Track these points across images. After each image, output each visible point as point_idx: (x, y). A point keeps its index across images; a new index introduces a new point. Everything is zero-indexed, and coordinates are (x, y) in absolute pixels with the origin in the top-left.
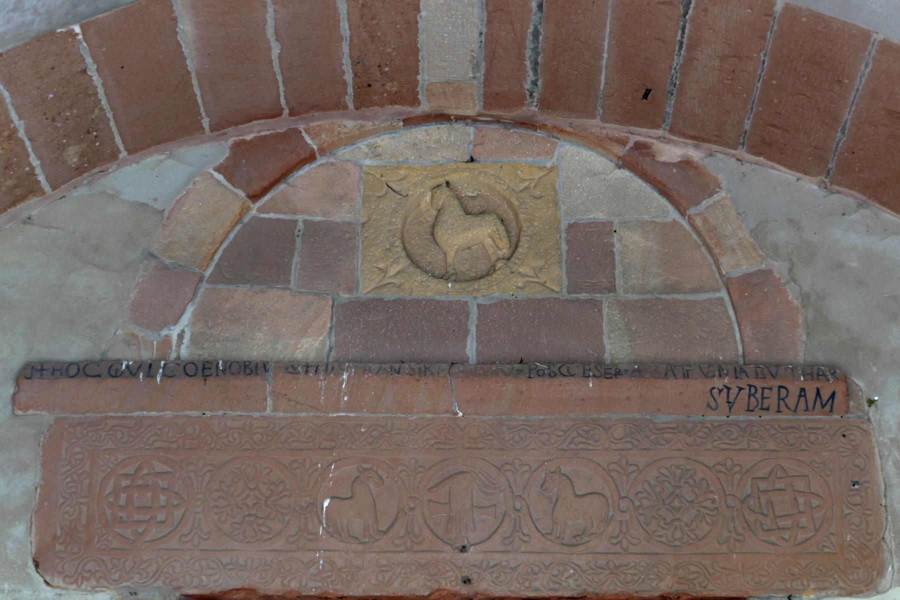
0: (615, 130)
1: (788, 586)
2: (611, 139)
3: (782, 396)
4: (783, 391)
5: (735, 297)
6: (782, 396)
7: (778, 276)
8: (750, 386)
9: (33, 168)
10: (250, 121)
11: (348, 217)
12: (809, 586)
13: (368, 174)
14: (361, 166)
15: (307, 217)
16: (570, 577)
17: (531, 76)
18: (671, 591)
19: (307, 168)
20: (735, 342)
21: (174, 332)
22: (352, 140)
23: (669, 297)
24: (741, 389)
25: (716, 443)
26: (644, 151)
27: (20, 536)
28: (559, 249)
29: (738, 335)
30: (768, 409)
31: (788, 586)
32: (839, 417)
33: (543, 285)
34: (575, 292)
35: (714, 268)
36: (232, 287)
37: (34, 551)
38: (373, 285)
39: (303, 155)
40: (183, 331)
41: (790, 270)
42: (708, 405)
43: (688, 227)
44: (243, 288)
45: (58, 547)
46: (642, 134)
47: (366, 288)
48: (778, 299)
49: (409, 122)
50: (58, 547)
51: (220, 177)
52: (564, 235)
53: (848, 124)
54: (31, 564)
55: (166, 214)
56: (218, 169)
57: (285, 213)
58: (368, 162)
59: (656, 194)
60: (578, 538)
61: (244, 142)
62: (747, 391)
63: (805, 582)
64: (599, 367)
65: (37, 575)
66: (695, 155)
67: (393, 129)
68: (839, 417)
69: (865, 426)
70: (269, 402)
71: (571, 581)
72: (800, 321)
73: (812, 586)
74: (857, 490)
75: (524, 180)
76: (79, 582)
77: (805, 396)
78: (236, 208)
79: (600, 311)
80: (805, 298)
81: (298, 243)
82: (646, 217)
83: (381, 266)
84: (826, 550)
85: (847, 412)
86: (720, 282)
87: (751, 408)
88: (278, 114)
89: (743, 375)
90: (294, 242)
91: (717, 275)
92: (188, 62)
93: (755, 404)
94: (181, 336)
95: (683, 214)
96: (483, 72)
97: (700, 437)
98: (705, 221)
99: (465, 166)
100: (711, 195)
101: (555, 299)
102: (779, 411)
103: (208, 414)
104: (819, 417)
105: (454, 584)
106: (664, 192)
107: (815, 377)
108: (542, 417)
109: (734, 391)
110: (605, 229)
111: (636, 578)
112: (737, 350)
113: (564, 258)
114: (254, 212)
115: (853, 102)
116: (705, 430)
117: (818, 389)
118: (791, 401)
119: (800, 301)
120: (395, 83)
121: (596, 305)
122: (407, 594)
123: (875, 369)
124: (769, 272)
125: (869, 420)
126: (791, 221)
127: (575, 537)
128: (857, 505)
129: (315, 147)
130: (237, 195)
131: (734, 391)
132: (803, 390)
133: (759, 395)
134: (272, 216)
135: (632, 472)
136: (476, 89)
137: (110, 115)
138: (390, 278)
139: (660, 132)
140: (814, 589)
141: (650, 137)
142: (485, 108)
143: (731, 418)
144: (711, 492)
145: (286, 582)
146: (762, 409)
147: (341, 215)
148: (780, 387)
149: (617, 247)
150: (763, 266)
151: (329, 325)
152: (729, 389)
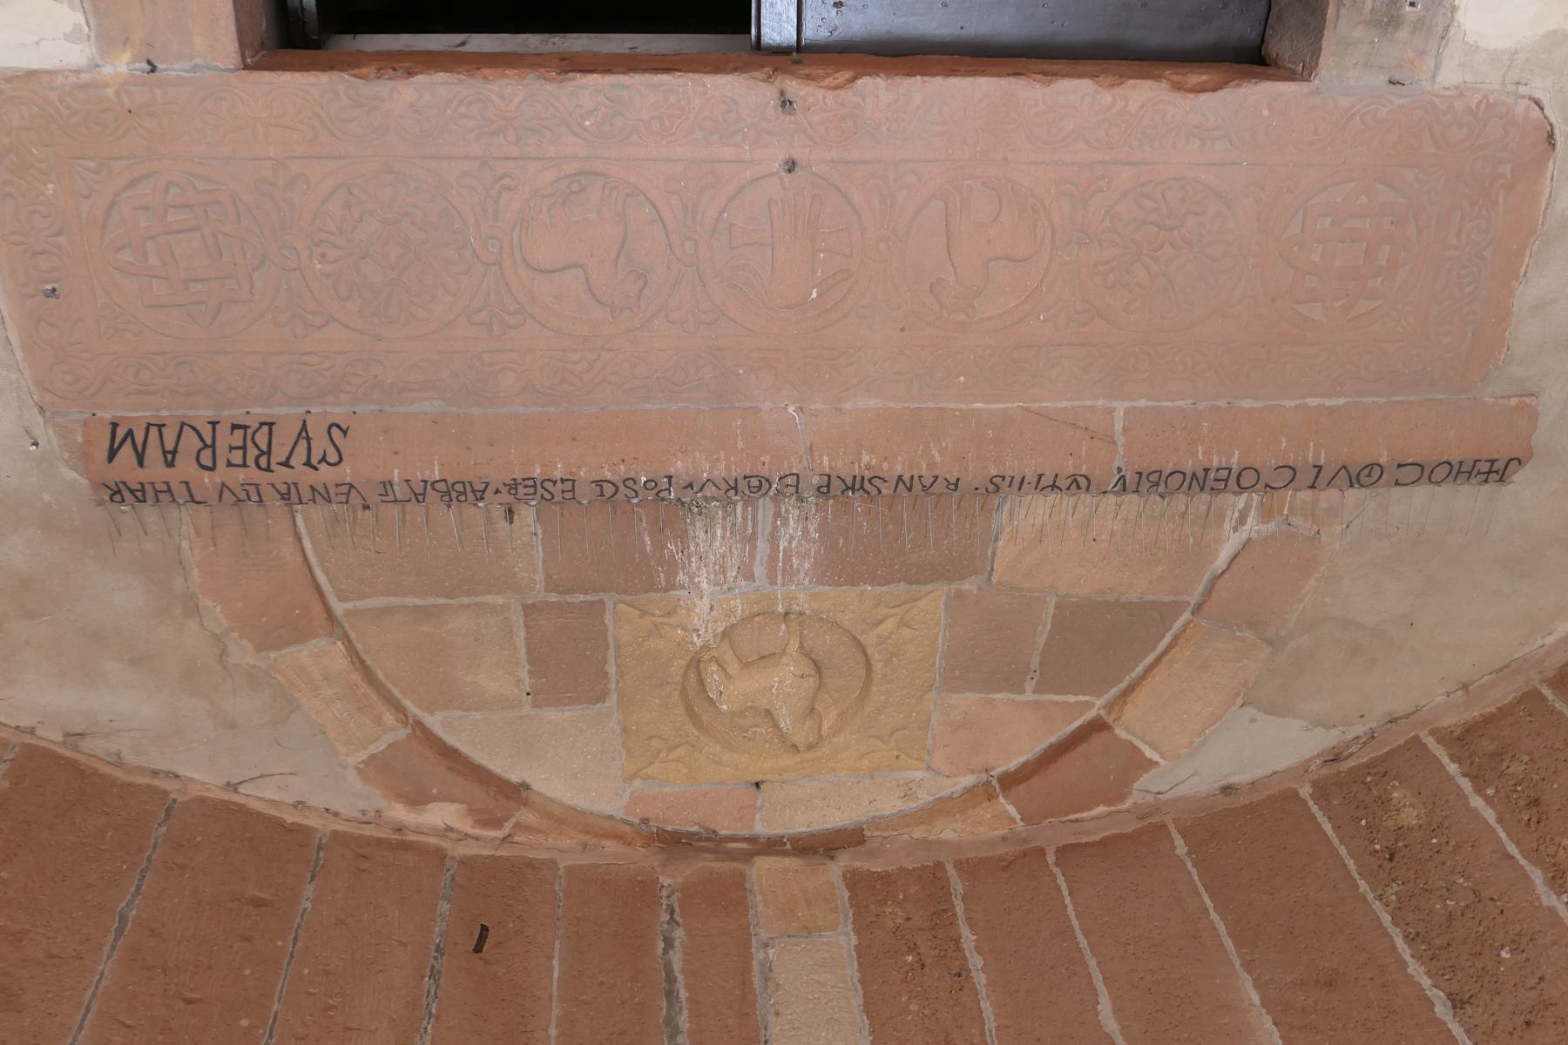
0: (537, 847)
1: (159, 93)
2: (539, 832)
3: (208, 452)
4: (206, 459)
5: (317, 608)
6: (208, 452)
7: (245, 642)
8: (268, 469)
9: (1479, 791)
10: (1104, 842)
11: (954, 699)
12: (117, 93)
13: (919, 759)
14: (929, 768)
15: (1018, 698)
16: (591, 112)
17: (677, 958)
18: (391, 84)
19: (1012, 765)
20: (310, 533)
21: (1252, 526)
22: (941, 808)
23: (431, 601)
24: (286, 464)
25: (326, 365)
26: (485, 816)
27: (1567, 193)
28: (618, 666)
29: (307, 544)
30: (234, 427)
31: (159, 93)
32: (100, 414)
33: (644, 613)
34: (594, 602)
35: (359, 647)
36: (1150, 597)
37: (1551, 164)
38: (921, 604)
39: (1021, 790)
40: (1235, 529)
41: (223, 653)
42: (345, 433)
43: (409, 704)
44: (1133, 597)
45: (1507, 170)
46: (484, 843)
47: (934, 600)
48: (240, 605)
49: (852, 838)
50: (1507, 170)
51: (1149, 754)
52: (613, 686)
53: (107, 949)
54: (1559, 139)
55: (1240, 701)
56: (1152, 764)
57: (1052, 702)
58: (918, 775)
59: (465, 749)
60: (575, 187)
61: (1108, 803)
62: (274, 460)
63: (126, 100)
64: (547, 496)
65: (1553, 120)
66: (400, 812)
67: (875, 823)
68: (100, 414)
69: (48, 398)
70: (1118, 426)
71: (589, 104)
72: (196, 573)
73: (110, 92)
74: (47, 282)
75: (678, 760)
76: (1483, 105)
77: (165, 453)
78: (1131, 712)
79: (548, 577)
80: (193, 609)
81: (1035, 662)
82: (478, 716)
83: (906, 632)
84: (92, 164)
85: (85, 423)
86: (347, 626)
87: (265, 429)
88: (1062, 851)
89: (284, 489)
90: (1041, 664)
91: (353, 636)
92: (1255, 998)
93: (257, 436)
94: (1242, 520)
95: (419, 725)
96: (754, 962)
97: (356, 375)
98: (378, 720)
99: (769, 777)
100: (373, 757)
101: (625, 592)
102: (214, 424)
103: (1222, 403)
104: (136, 414)
105: (811, 100)
106: (451, 756)
107: (148, 488)
108: (647, 406)
109: (299, 458)
110: (542, 696)
111: (463, 109)
112: (306, 520)
113: (611, 653)
114: (1099, 702)
115: (88, 1009)
116: (349, 388)
117: (141, 464)
118: (190, 442)
119: (201, 605)
120: (890, 924)
121: (552, 585)
122: (898, 79)
123: (47, 497)
124: (262, 647)
125: (42, 410)
126: (233, 726)
127: (583, 190)
128: (41, 253)
129: (1002, 800)
130: (1128, 730)
131: (299, 458)
132: (170, 464)
133: (252, 452)
134: (1071, 698)
135: (479, 310)
136: (763, 914)
137: (1363, 886)
138: (894, 615)
139: (462, 850)
140: (106, 85)
141: (477, 839)
142: (743, 875)
143: (301, 410)
144: (328, 276)
145: (1120, 104)
146: (245, 427)
147: (965, 701)
148: (213, 469)
149: (523, 673)
150: (272, 655)
151: (1000, 543)
152: (308, 463)
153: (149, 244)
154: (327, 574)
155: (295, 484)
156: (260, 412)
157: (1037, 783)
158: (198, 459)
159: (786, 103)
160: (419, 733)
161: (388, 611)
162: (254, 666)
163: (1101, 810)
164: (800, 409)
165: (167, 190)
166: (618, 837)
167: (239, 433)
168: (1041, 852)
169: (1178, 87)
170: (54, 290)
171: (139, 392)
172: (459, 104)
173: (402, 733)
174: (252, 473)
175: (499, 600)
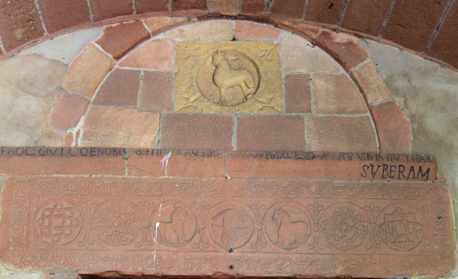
1: (404, 272)
4: (402, 168)
8: (384, 165)
21: (74, 131)
28: (281, 89)
30: (393, 177)
32: (431, 182)
33: (273, 108)
38: (182, 107)
39: (144, 35)
40: (79, 131)
41: (405, 102)
42: (362, 175)
43: (349, 78)
47: (178, 107)
49: (201, 18)
50: (11, 248)
51: (99, 47)
56: (98, 42)
58: (178, 40)
59: (332, 60)
60: (292, 246)
61: (112, 28)
62: (382, 167)
63: (413, 270)
66: (355, 40)
71: (288, 268)
73: (417, 273)
75: (262, 51)
77: (413, 170)
80: (413, 117)
82: (328, 72)
84: (424, 254)
87: (384, 176)
90: (139, 82)
91: (365, 104)
93: (387, 174)
94: (78, 133)
95: (347, 71)
98: (360, 75)
99: (230, 42)
100: (362, 61)
102: (399, 178)
103: (94, 176)
106: (337, 59)
109: (375, 168)
111: (323, 267)
113: (284, 93)
114: (117, 66)
117: (420, 167)
118: (406, 173)
124: (393, 103)
129: (150, 31)
130: (108, 57)
132: (412, 167)
133: (388, 170)
134: (127, 68)
139: (335, 26)
145: (135, 267)
146: (390, 177)
147: (164, 68)
148: (400, 166)
149: (312, 87)
150: (390, 100)
151: (158, 129)
152: (373, 166)
153: (411, 231)
154: (371, 126)
155: (377, 160)
156: (385, 182)
157: (139, 38)
158: (404, 167)
159: (231, 267)
160: (347, 68)
161: (353, 112)
162: (396, 96)
163: (114, 25)
164: (226, 178)
165: (405, 247)
166: (283, 25)
167: (392, 175)
168: (137, 13)
169: (117, 272)
170: (439, 219)
171: (419, 188)
172: (324, 268)
173: (353, 69)
174: (389, 163)
175: (321, 115)
